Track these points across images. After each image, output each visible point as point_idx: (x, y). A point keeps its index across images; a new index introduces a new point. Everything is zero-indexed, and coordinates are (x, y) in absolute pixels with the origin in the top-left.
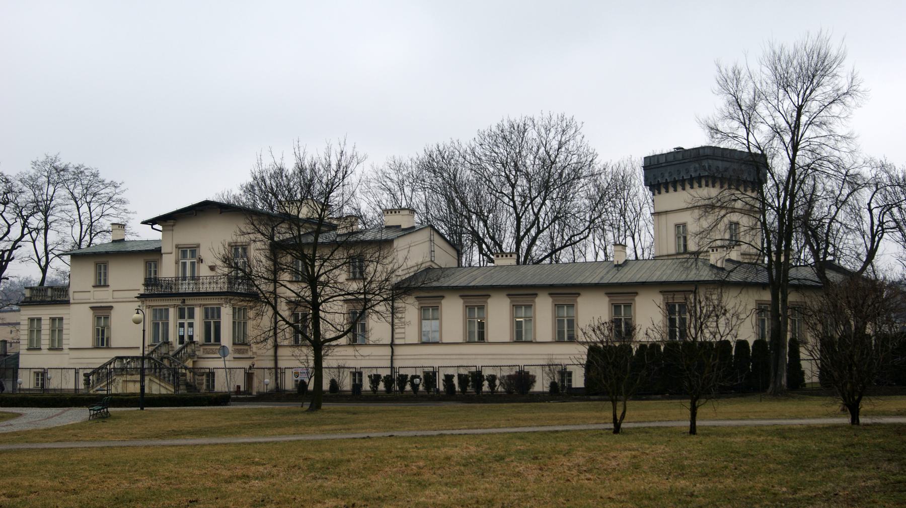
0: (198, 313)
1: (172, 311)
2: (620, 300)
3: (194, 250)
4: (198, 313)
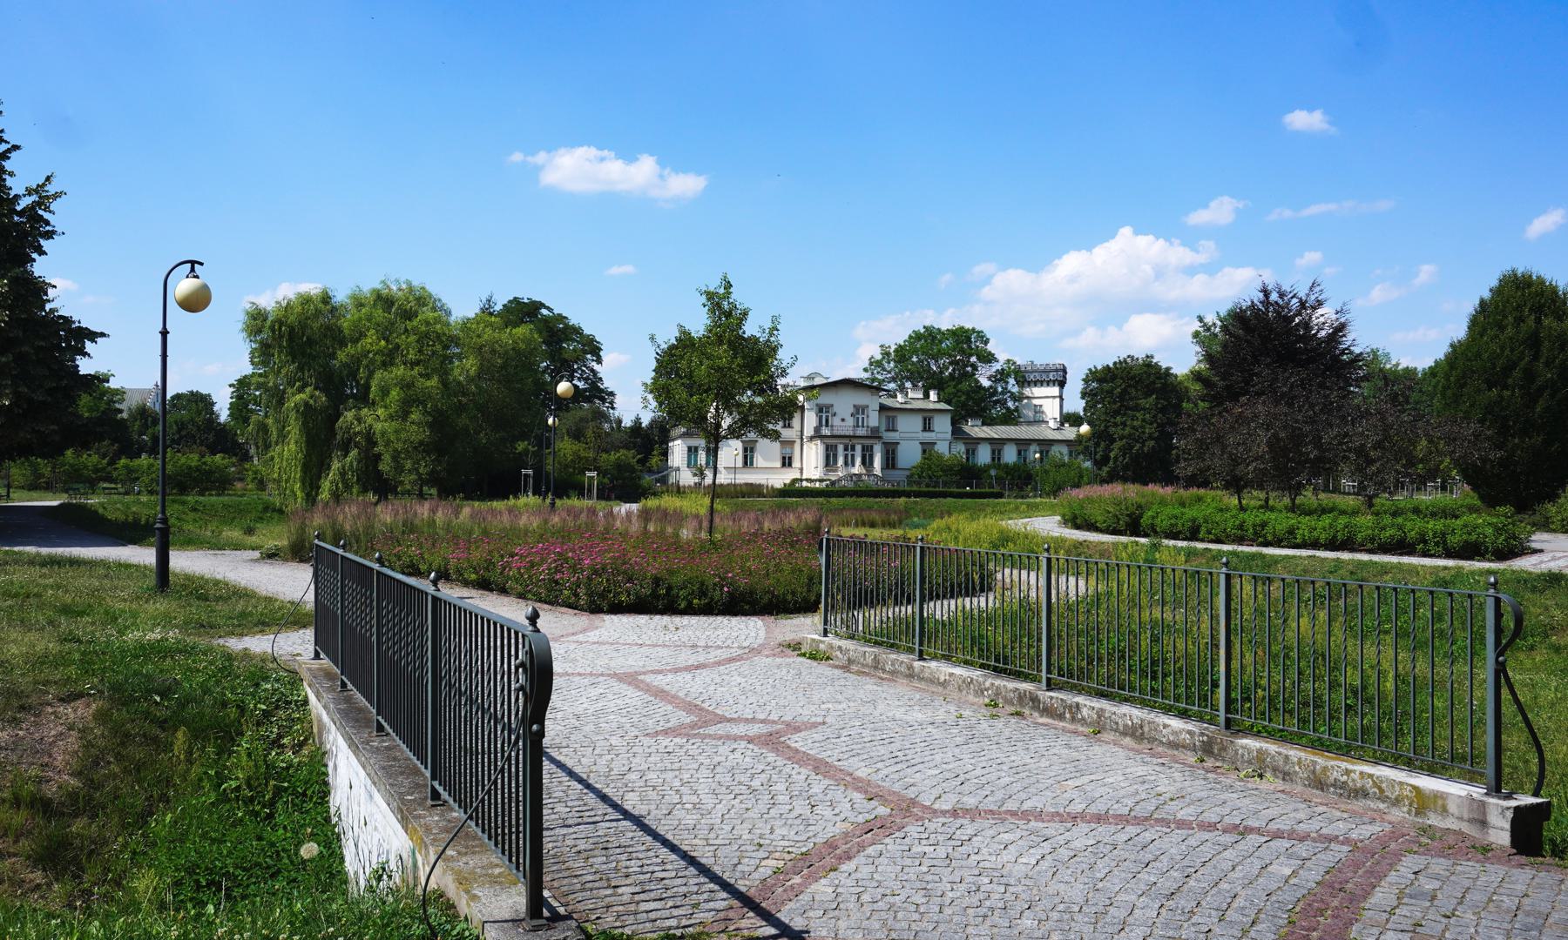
0: (859, 448)
1: (841, 448)
2: (997, 447)
3: (829, 407)
4: (859, 448)
